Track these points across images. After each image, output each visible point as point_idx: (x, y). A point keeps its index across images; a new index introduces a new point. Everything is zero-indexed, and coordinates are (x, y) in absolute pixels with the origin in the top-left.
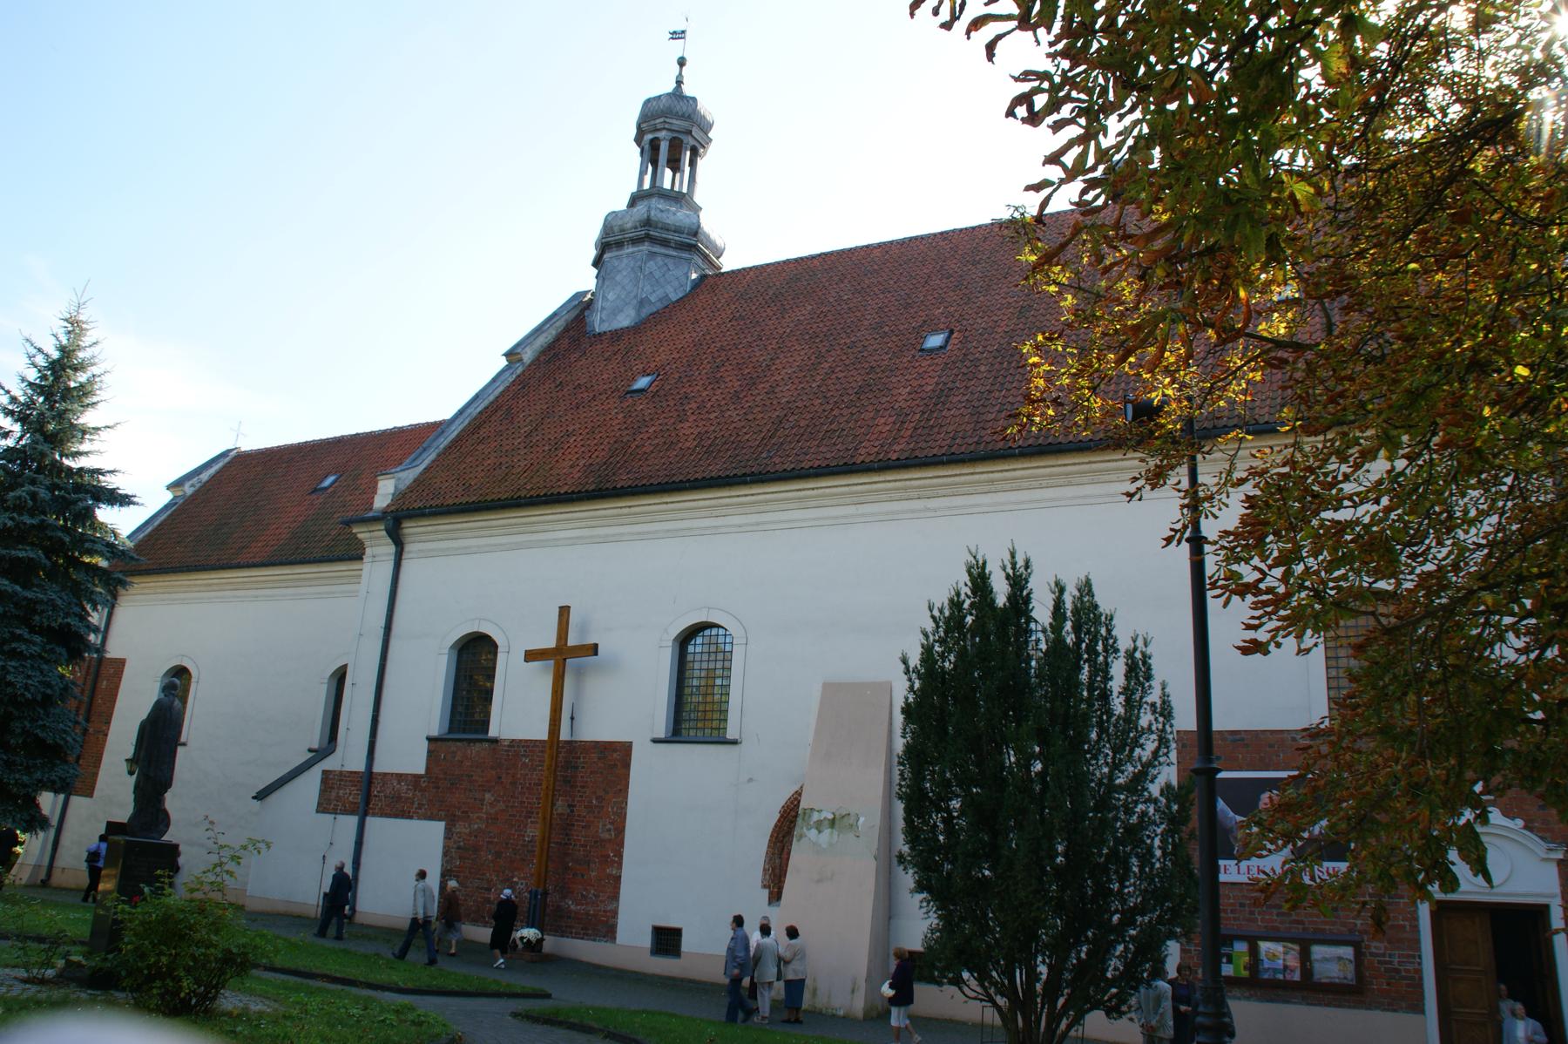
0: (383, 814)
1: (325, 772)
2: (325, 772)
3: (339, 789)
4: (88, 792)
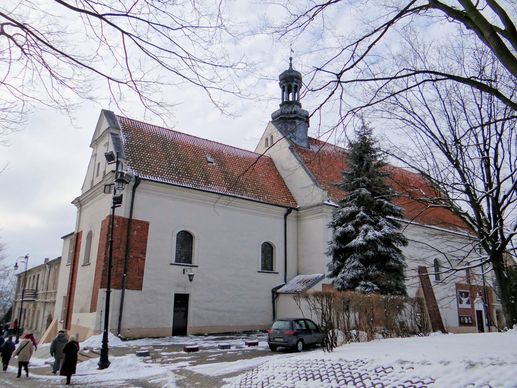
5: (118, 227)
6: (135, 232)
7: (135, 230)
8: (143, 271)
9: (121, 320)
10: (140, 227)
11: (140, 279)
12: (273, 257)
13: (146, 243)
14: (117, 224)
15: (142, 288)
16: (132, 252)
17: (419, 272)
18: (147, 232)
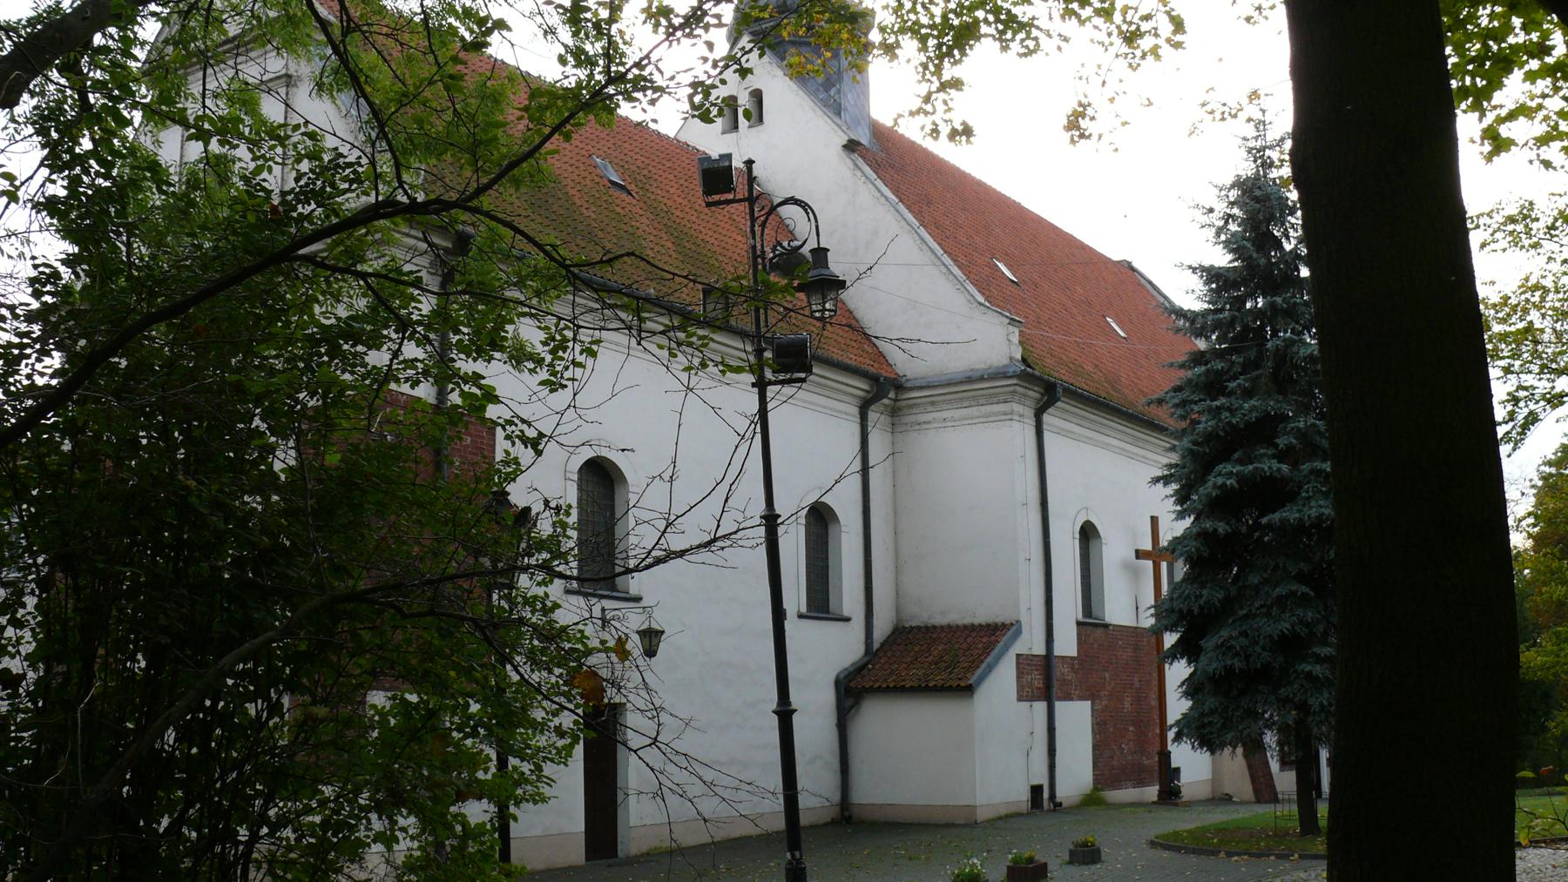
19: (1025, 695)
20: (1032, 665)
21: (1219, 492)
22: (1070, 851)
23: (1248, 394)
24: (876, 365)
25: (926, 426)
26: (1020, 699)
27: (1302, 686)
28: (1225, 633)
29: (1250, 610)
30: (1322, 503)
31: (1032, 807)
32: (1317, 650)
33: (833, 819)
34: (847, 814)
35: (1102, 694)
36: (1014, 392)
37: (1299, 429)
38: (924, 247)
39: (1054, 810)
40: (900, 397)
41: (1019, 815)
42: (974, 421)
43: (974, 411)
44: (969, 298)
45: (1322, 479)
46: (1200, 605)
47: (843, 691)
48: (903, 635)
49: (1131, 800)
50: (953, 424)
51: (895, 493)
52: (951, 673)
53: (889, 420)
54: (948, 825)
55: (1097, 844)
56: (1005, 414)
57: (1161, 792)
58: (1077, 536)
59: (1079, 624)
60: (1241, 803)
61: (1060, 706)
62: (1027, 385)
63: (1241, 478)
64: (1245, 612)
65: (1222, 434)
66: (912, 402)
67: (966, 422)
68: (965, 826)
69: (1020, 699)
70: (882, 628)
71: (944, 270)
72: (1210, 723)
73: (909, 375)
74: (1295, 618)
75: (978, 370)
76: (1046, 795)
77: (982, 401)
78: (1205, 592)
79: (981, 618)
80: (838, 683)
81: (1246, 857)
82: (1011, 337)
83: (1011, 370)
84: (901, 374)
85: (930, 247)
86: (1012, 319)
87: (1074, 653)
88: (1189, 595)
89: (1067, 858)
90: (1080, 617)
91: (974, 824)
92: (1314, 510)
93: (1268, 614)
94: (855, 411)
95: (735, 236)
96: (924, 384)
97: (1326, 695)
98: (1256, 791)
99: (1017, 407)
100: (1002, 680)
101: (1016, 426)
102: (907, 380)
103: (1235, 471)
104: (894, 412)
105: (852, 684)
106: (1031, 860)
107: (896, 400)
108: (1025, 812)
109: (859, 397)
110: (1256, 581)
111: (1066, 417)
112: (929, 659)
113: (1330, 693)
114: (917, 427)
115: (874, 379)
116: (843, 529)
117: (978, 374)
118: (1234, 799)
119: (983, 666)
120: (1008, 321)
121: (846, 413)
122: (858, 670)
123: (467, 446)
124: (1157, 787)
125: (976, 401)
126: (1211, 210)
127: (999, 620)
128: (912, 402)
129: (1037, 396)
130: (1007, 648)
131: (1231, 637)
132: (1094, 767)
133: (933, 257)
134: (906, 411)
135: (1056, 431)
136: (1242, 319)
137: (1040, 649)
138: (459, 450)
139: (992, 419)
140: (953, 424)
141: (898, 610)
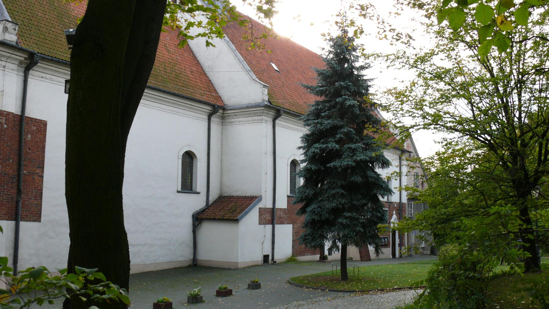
0: (279, 224)
1: (260, 208)
2: (260, 208)
3: (264, 215)
4: (36, 217)
5: (7, 129)
6: (29, 136)
7: (27, 134)
8: (42, 193)
9: (17, 263)
10: (35, 128)
11: (38, 204)
12: (192, 182)
13: (44, 152)
14: (5, 124)
15: (40, 217)
16: (26, 165)
17: (20, 63)
18: (45, 137)
19: (262, 222)
20: (266, 212)
21: (313, 154)
22: (249, 284)
23: (329, 117)
24: (215, 101)
25: (233, 123)
26: (260, 224)
27: (339, 227)
28: (313, 206)
29: (323, 198)
30: (349, 160)
31: (264, 263)
32: (345, 214)
33: (189, 265)
34: (195, 263)
35: (298, 222)
36: (263, 112)
37: (345, 132)
38: (236, 58)
39: (273, 264)
40: (225, 113)
41: (258, 265)
42: (250, 122)
43: (249, 118)
44: (250, 77)
45: (351, 151)
46: (305, 196)
47: (195, 218)
48: (223, 200)
49: (309, 260)
50: (242, 123)
51: (222, 147)
52: (232, 214)
53: (221, 121)
54: (229, 269)
55: (259, 282)
56: (260, 120)
57: (320, 257)
58: (289, 165)
59: (288, 196)
60: (356, 261)
61: (277, 227)
62: (269, 110)
63: (322, 150)
64: (321, 199)
65: (317, 132)
66: (229, 114)
67: (247, 122)
68: (235, 269)
69: (260, 224)
70: (213, 196)
71: (242, 67)
72: (308, 239)
73: (229, 104)
74: (338, 202)
75: (251, 104)
76: (270, 258)
77: (252, 115)
78: (307, 191)
79: (248, 194)
80: (193, 216)
81: (311, 289)
82: (264, 92)
83: (262, 104)
84: (226, 104)
85: (238, 58)
86: (264, 85)
87: (286, 207)
88: (302, 191)
89: (247, 287)
90: (289, 194)
91: (237, 269)
92: (346, 162)
93: (329, 200)
94: (206, 117)
95: (164, 52)
96: (232, 108)
97: (347, 231)
98: (361, 257)
99: (264, 118)
100: (253, 216)
101: (264, 125)
102: (228, 106)
103: (319, 147)
104: (223, 118)
105: (199, 217)
106: (225, 288)
107: (223, 114)
108: (260, 264)
109: (208, 112)
110: (326, 188)
111: (287, 121)
112: (227, 209)
113: (349, 230)
114: (230, 124)
115: (213, 106)
116: (198, 160)
117: (251, 105)
118: (353, 259)
119: (244, 212)
120: (263, 86)
121: (202, 118)
122: (203, 211)
123: (34, 130)
124: (319, 255)
125: (250, 115)
126: (323, 49)
127: (254, 195)
128: (229, 114)
129: (274, 114)
130: (254, 206)
131: (314, 208)
132: (292, 248)
133: (239, 62)
134: (227, 118)
135: (282, 126)
136: (330, 90)
137: (270, 206)
138: (31, 132)
139: (256, 122)
140: (242, 123)
141: (221, 190)
